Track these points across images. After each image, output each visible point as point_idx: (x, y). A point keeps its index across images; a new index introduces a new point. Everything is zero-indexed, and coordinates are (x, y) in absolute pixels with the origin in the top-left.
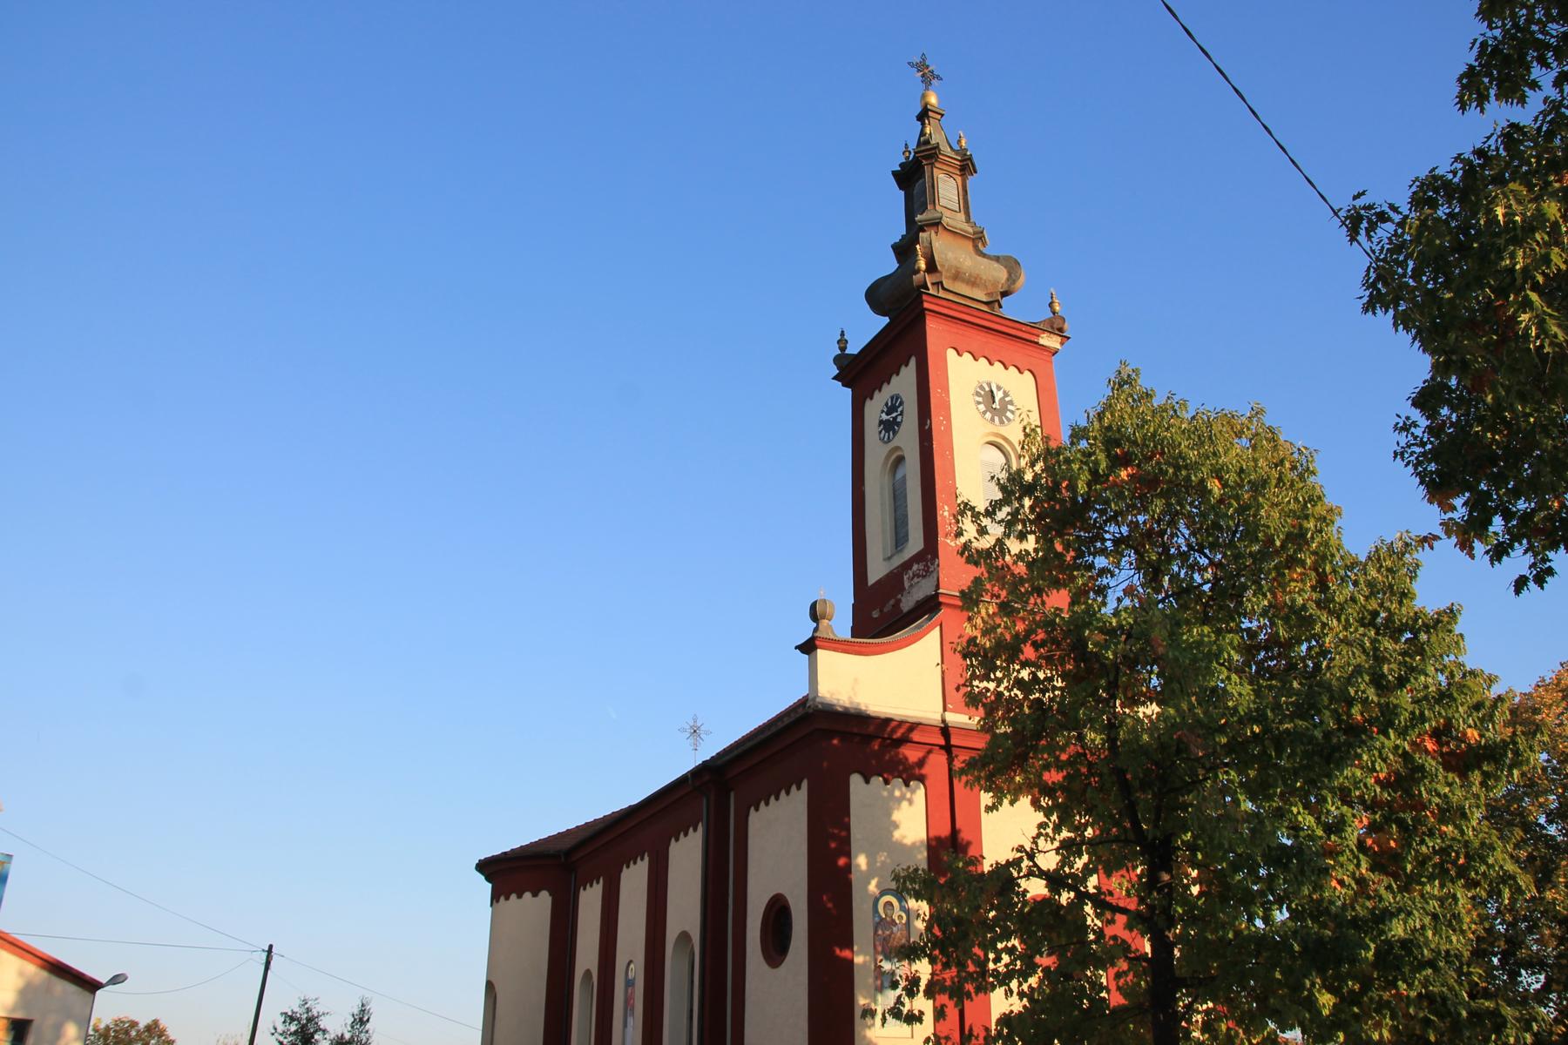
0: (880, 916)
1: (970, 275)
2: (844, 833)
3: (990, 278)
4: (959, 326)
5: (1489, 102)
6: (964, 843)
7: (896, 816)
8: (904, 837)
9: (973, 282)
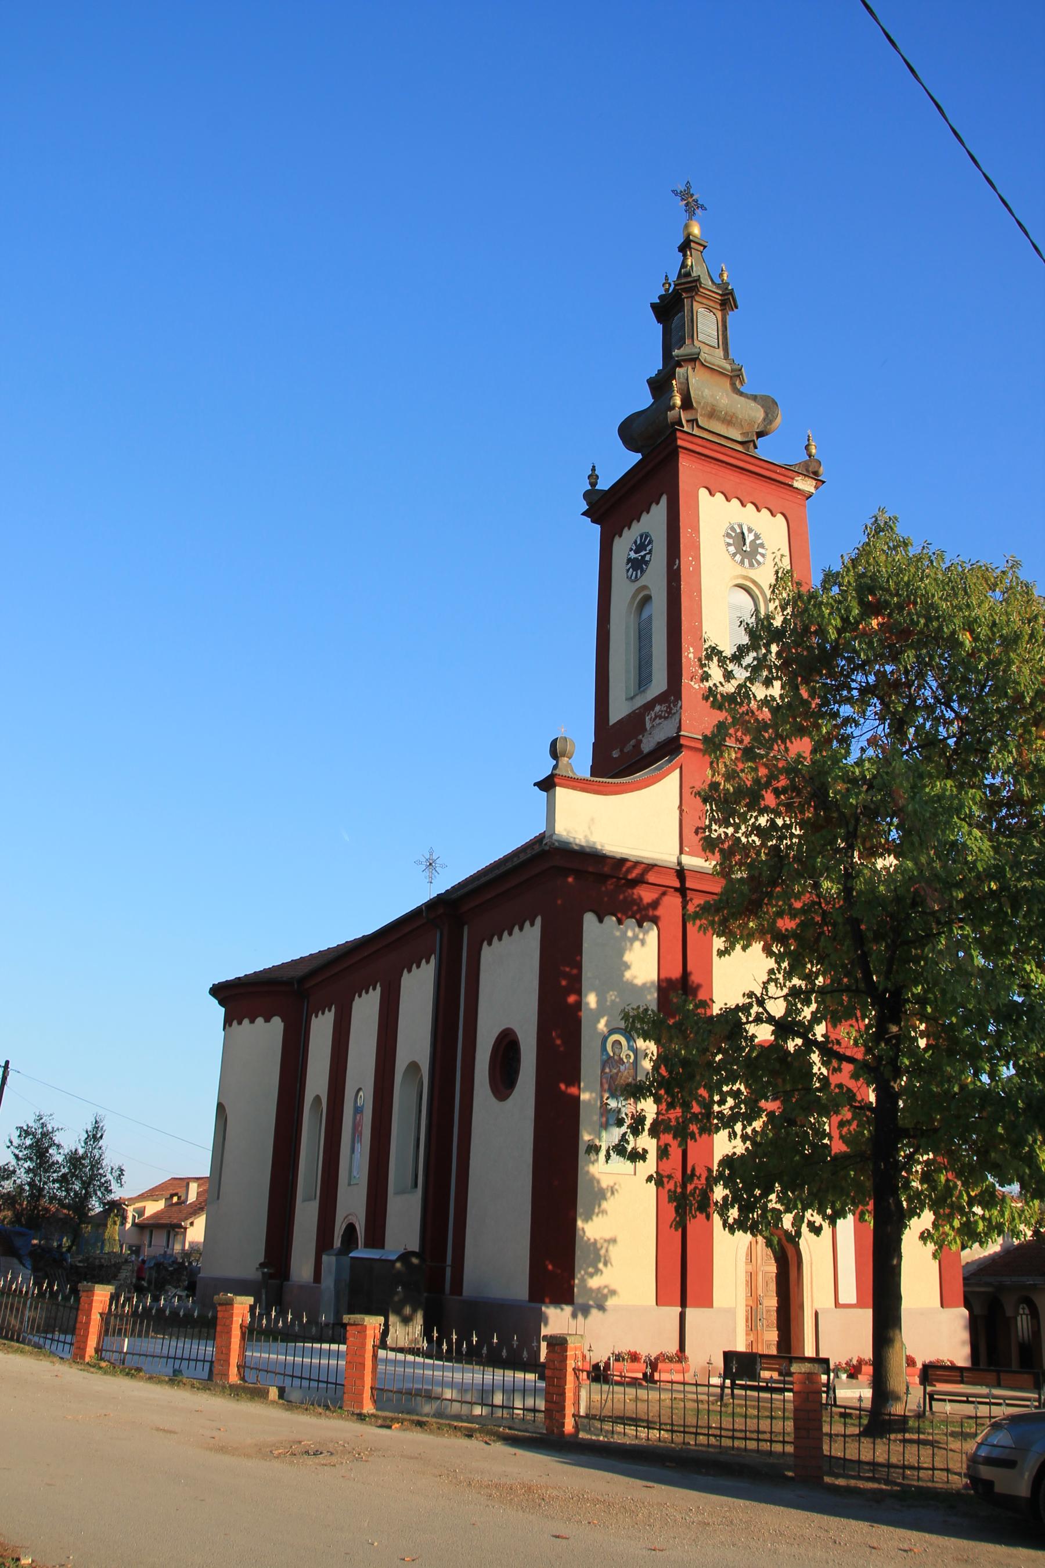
0: (608, 1053)
1: (726, 414)
2: (575, 971)
3: (747, 417)
6: (694, 985)
7: (628, 957)
8: (635, 977)
9: (729, 420)
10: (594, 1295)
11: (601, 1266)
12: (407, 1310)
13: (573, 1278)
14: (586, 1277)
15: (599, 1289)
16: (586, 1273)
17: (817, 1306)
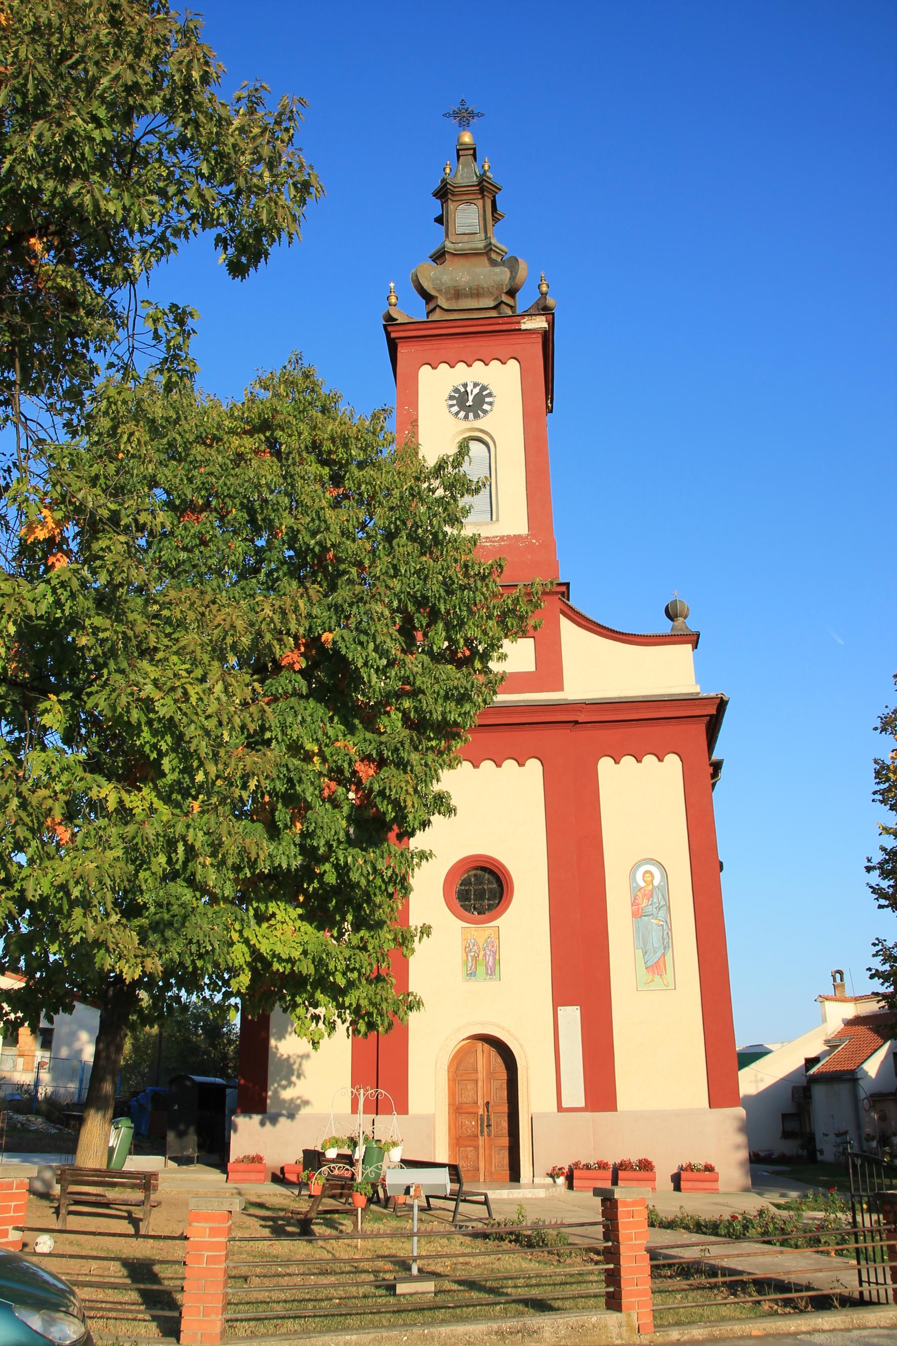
1: (470, 289)
3: (492, 284)
4: (434, 342)
5: (256, 269)
9: (477, 293)
10: (287, 1105)
11: (294, 1078)
12: (182, 1127)
13: (266, 1090)
14: (279, 1089)
15: (292, 1100)
16: (279, 1085)
17: (534, 1110)
